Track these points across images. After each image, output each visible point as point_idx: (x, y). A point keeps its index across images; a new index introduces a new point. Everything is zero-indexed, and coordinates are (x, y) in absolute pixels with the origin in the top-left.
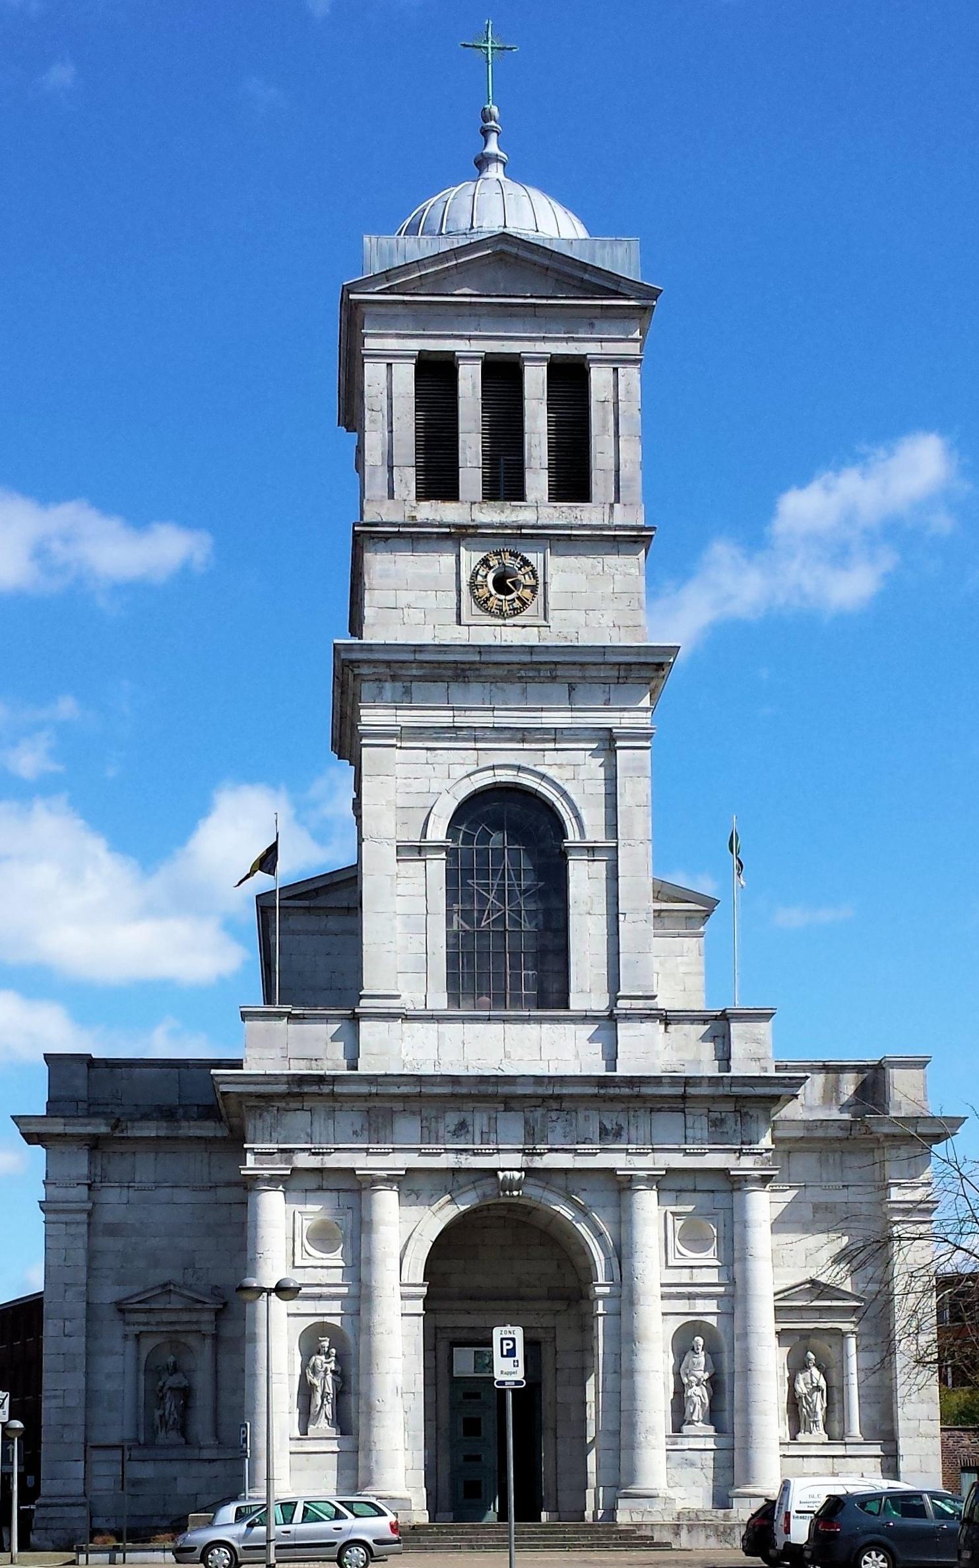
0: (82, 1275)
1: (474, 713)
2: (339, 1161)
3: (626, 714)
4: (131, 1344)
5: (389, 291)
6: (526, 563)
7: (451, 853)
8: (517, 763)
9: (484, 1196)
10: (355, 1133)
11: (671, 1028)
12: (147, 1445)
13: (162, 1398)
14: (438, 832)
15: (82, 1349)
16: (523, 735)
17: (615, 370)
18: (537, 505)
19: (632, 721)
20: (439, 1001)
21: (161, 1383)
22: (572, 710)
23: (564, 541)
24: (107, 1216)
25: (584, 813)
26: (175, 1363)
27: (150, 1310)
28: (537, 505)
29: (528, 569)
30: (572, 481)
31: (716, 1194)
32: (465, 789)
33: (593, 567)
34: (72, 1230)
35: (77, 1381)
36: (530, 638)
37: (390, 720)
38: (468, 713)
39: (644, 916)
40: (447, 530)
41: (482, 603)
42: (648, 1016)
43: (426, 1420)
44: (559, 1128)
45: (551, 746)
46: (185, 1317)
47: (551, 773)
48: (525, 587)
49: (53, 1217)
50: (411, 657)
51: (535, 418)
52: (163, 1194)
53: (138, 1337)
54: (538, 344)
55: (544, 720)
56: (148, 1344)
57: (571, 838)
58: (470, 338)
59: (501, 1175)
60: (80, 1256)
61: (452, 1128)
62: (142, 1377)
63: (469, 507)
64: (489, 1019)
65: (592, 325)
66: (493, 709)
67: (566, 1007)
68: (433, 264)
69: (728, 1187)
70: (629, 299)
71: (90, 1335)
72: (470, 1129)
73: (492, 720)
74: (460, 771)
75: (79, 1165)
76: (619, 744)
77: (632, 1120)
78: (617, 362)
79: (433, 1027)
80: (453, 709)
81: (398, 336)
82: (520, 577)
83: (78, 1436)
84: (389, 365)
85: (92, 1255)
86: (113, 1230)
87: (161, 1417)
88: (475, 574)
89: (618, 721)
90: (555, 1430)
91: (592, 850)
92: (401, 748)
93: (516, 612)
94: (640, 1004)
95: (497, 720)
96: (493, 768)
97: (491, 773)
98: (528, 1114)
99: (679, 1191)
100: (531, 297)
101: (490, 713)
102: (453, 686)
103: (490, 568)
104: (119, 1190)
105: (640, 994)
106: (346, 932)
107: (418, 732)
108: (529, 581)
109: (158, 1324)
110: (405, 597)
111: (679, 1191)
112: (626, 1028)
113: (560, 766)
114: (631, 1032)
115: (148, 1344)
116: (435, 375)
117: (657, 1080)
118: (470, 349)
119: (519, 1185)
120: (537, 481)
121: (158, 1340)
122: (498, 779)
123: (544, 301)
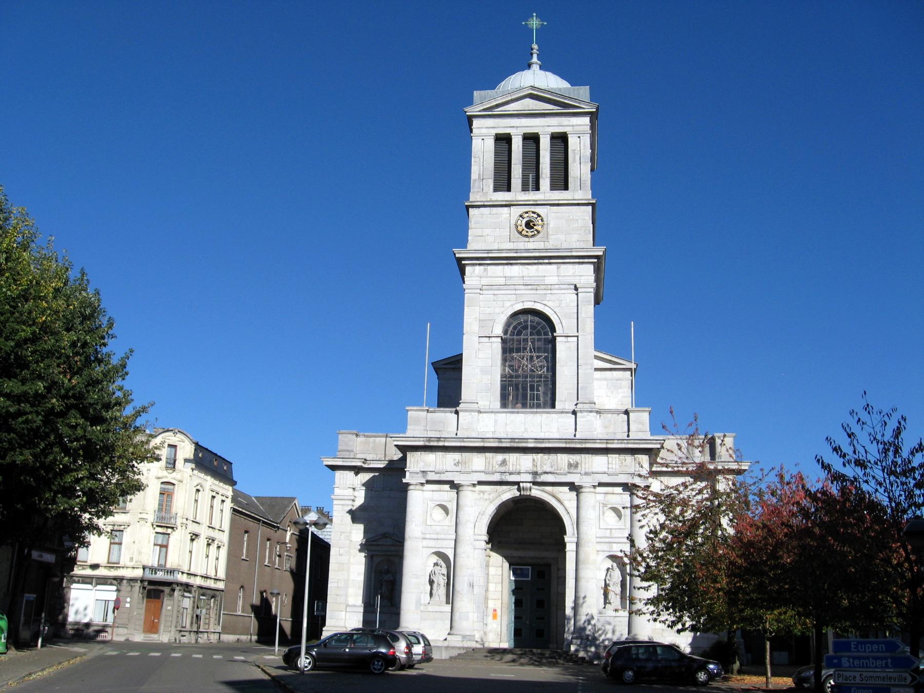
6: (539, 216)
14: (499, 330)
17: (628, 436)
18: (545, 192)
20: (497, 404)
25: (563, 322)
27: (377, 545)
31: (512, 208)
36: (541, 245)
42: (591, 412)
45: (549, 292)
46: (393, 548)
51: (544, 157)
59: (521, 485)
64: (518, 413)
79: (493, 415)
106: (454, 369)
110: (487, 231)
112: (582, 417)
116: (503, 140)
120: (545, 182)
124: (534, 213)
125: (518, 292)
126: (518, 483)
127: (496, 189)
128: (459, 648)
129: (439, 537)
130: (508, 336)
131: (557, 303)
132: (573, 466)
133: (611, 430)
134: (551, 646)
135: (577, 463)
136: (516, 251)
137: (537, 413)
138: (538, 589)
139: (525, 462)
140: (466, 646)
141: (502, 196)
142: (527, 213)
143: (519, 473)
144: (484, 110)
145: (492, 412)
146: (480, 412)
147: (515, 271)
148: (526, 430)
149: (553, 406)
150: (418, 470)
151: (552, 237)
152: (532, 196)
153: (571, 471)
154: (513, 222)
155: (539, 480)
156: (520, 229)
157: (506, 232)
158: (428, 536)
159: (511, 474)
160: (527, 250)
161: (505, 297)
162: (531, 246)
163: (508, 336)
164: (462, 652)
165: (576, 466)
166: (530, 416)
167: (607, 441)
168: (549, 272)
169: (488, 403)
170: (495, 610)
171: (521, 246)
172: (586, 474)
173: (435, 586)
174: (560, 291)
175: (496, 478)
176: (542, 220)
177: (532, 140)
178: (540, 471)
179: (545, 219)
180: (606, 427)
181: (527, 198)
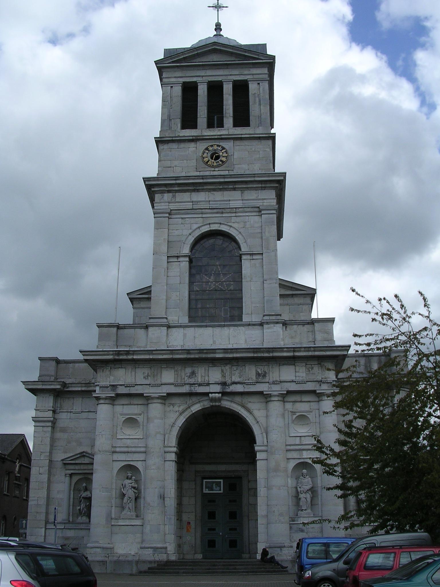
0: (48, 449)
2: (137, 390)
3: (265, 201)
4: (68, 479)
5: (173, 62)
9: (204, 405)
10: (144, 378)
12: (73, 522)
13: (81, 502)
14: (186, 250)
15: (46, 480)
16: (221, 211)
17: (259, 84)
18: (228, 127)
20: (185, 320)
21: (79, 495)
24: (60, 424)
26: (86, 487)
28: (228, 127)
31: (311, 403)
34: (45, 429)
35: (44, 493)
39: (275, 281)
42: (277, 323)
44: (237, 372)
45: (234, 215)
47: (235, 225)
48: (223, 157)
49: (38, 424)
50: (174, 182)
52: (84, 415)
53: (71, 475)
56: (75, 479)
57: (243, 250)
60: (48, 441)
61: (188, 374)
62: (72, 493)
63: (202, 129)
64: (206, 326)
69: (317, 399)
70: (263, 60)
71: (50, 473)
72: (197, 375)
74: (195, 226)
75: (49, 402)
76: (263, 212)
77: (271, 370)
79: (182, 330)
81: (175, 77)
82: (221, 154)
83: (43, 517)
84: (172, 87)
85: (53, 440)
86: (64, 430)
87: (80, 510)
90: (248, 516)
94: (274, 318)
98: (223, 368)
99: (294, 402)
102: (193, 193)
104: (66, 413)
105: (274, 314)
108: (225, 155)
109: (79, 470)
110: (176, 163)
111: (294, 402)
113: (238, 223)
115: (75, 479)
118: (202, 79)
119: (219, 400)
121: (79, 477)
122: (212, 229)
123: (230, 62)
125: (204, 216)
126: (207, 394)
127: (183, 127)
128: (150, 562)
129: (130, 450)
131: (242, 225)
132: (261, 376)
133: (297, 340)
134: (244, 556)
135: (265, 373)
136: (203, 177)
137: (224, 326)
138: (230, 501)
139: (215, 375)
140: (157, 559)
141: (189, 133)
142: (212, 146)
143: (208, 384)
145: (181, 327)
147: (201, 197)
148: (214, 342)
150: (108, 384)
152: (216, 132)
153: (260, 380)
155: (228, 390)
156: (206, 160)
157: (193, 163)
158: (118, 450)
159: (200, 385)
160: (214, 177)
161: (193, 221)
164: (153, 565)
165: (264, 376)
166: (217, 330)
167: (294, 350)
168: (234, 199)
170: (189, 523)
172: (274, 383)
173: (219, 225)
174: (244, 214)
175: (185, 389)
176: (226, 152)
177: (215, 89)
178: (229, 381)
179: (229, 152)
180: (292, 338)
181: (212, 134)
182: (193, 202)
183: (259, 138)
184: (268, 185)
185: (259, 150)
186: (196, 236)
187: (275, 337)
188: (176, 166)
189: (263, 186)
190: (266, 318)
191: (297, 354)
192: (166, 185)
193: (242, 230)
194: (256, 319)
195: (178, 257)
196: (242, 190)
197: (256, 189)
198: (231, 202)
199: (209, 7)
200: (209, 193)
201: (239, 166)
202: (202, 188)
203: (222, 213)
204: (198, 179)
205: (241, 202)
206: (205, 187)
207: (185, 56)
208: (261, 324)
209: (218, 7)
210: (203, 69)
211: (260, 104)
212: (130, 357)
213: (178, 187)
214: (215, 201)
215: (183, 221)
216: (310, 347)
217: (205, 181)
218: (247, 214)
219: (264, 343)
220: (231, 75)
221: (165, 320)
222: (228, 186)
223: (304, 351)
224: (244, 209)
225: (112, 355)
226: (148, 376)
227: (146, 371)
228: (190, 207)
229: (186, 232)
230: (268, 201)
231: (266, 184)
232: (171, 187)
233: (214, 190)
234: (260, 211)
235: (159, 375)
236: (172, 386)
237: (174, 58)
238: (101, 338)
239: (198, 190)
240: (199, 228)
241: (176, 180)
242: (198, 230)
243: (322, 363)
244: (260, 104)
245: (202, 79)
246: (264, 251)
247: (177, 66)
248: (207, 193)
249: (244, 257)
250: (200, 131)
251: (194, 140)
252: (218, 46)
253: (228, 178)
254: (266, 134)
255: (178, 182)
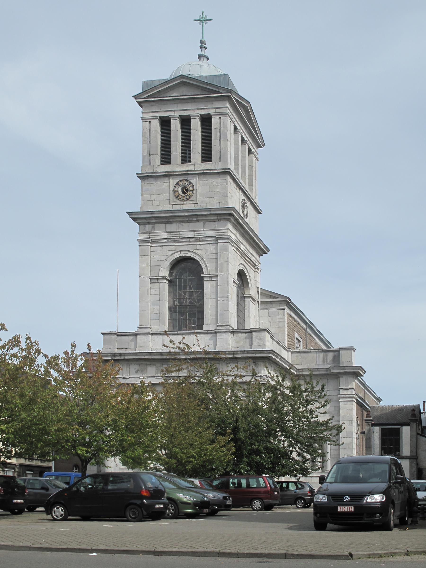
1: (173, 233)
3: (221, 231)
5: (148, 97)
6: (191, 183)
7: (170, 281)
8: (187, 249)
10: (136, 372)
11: (235, 335)
14: (165, 273)
16: (189, 240)
17: (220, 118)
18: (197, 162)
19: (223, 233)
22: (204, 231)
23: (201, 174)
28: (197, 162)
29: (191, 185)
30: (207, 156)
32: (172, 259)
33: (212, 183)
36: (192, 207)
37: (148, 237)
38: (171, 234)
40: (165, 174)
41: (177, 197)
42: (226, 332)
43: (422, 528)
45: (198, 243)
47: (199, 252)
48: (190, 191)
54: (196, 111)
55: (195, 235)
57: (204, 273)
58: (174, 111)
63: (176, 165)
65: (213, 104)
66: (179, 232)
67: (202, 329)
68: (161, 87)
70: (221, 93)
73: (179, 235)
74: (170, 253)
76: (219, 241)
78: (220, 115)
80: (167, 232)
81: (153, 112)
82: (188, 188)
84: (150, 122)
88: (175, 188)
89: (218, 234)
91: (211, 277)
92: (152, 246)
93: (187, 199)
95: (180, 235)
96: (180, 251)
97: (179, 253)
100: (191, 95)
101: (178, 233)
102: (167, 225)
103: (179, 185)
105: (224, 324)
107: (157, 240)
110: (154, 197)
112: (220, 336)
114: (220, 337)
117: (224, 352)
118: (174, 113)
123: (195, 96)
124: (187, 181)
125: (176, 244)
127: (162, 163)
130: (173, 277)
141: (166, 168)
142: (181, 181)
144: (148, 97)
146: (152, 335)
147: (173, 228)
149: (201, 327)
151: (199, 201)
154: (172, 189)
157: (167, 197)
162: (185, 207)
163: (173, 277)
168: (198, 230)
169: (157, 327)
171: (178, 208)
182: (167, 232)
183: (218, 173)
184: (223, 218)
185: (218, 184)
186: (171, 260)
187: (228, 343)
188: (154, 200)
189: (219, 218)
190: (219, 328)
191: (236, 356)
192: (145, 218)
193: (204, 257)
194: (212, 328)
195: (158, 279)
196: (204, 222)
197: (214, 220)
198: (195, 233)
199: (195, 20)
200: (179, 225)
201: (203, 199)
202: (173, 220)
203: (190, 242)
204: (168, 213)
205: (203, 232)
206: (176, 220)
207: (158, 90)
208: (215, 333)
209: (203, 20)
210: (175, 103)
211: (220, 140)
212: (122, 358)
213: (155, 219)
214: (183, 232)
215: (161, 248)
216: (244, 351)
217: (173, 215)
218: (208, 243)
219: (137, 349)
220: (197, 109)
221: (150, 330)
222: (192, 218)
223: (241, 354)
224: (205, 238)
225: (110, 356)
226: (138, 371)
227: (137, 367)
228: (165, 237)
229: (163, 258)
230: (223, 231)
231: (221, 216)
232: (150, 220)
233: (183, 222)
234: (217, 240)
235: (145, 370)
236: (154, 379)
237: (150, 92)
238: (105, 342)
239: (170, 222)
240: (173, 254)
241: (152, 214)
242: (172, 256)
243: (257, 362)
244: (220, 140)
245: (174, 113)
246: (219, 274)
247: (153, 101)
248: (178, 224)
249: (205, 279)
250: (173, 166)
251: (168, 175)
252: (185, 79)
253: (190, 212)
254: (223, 169)
255: (153, 215)
